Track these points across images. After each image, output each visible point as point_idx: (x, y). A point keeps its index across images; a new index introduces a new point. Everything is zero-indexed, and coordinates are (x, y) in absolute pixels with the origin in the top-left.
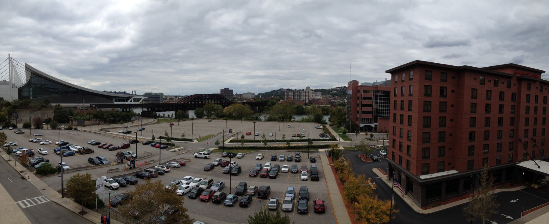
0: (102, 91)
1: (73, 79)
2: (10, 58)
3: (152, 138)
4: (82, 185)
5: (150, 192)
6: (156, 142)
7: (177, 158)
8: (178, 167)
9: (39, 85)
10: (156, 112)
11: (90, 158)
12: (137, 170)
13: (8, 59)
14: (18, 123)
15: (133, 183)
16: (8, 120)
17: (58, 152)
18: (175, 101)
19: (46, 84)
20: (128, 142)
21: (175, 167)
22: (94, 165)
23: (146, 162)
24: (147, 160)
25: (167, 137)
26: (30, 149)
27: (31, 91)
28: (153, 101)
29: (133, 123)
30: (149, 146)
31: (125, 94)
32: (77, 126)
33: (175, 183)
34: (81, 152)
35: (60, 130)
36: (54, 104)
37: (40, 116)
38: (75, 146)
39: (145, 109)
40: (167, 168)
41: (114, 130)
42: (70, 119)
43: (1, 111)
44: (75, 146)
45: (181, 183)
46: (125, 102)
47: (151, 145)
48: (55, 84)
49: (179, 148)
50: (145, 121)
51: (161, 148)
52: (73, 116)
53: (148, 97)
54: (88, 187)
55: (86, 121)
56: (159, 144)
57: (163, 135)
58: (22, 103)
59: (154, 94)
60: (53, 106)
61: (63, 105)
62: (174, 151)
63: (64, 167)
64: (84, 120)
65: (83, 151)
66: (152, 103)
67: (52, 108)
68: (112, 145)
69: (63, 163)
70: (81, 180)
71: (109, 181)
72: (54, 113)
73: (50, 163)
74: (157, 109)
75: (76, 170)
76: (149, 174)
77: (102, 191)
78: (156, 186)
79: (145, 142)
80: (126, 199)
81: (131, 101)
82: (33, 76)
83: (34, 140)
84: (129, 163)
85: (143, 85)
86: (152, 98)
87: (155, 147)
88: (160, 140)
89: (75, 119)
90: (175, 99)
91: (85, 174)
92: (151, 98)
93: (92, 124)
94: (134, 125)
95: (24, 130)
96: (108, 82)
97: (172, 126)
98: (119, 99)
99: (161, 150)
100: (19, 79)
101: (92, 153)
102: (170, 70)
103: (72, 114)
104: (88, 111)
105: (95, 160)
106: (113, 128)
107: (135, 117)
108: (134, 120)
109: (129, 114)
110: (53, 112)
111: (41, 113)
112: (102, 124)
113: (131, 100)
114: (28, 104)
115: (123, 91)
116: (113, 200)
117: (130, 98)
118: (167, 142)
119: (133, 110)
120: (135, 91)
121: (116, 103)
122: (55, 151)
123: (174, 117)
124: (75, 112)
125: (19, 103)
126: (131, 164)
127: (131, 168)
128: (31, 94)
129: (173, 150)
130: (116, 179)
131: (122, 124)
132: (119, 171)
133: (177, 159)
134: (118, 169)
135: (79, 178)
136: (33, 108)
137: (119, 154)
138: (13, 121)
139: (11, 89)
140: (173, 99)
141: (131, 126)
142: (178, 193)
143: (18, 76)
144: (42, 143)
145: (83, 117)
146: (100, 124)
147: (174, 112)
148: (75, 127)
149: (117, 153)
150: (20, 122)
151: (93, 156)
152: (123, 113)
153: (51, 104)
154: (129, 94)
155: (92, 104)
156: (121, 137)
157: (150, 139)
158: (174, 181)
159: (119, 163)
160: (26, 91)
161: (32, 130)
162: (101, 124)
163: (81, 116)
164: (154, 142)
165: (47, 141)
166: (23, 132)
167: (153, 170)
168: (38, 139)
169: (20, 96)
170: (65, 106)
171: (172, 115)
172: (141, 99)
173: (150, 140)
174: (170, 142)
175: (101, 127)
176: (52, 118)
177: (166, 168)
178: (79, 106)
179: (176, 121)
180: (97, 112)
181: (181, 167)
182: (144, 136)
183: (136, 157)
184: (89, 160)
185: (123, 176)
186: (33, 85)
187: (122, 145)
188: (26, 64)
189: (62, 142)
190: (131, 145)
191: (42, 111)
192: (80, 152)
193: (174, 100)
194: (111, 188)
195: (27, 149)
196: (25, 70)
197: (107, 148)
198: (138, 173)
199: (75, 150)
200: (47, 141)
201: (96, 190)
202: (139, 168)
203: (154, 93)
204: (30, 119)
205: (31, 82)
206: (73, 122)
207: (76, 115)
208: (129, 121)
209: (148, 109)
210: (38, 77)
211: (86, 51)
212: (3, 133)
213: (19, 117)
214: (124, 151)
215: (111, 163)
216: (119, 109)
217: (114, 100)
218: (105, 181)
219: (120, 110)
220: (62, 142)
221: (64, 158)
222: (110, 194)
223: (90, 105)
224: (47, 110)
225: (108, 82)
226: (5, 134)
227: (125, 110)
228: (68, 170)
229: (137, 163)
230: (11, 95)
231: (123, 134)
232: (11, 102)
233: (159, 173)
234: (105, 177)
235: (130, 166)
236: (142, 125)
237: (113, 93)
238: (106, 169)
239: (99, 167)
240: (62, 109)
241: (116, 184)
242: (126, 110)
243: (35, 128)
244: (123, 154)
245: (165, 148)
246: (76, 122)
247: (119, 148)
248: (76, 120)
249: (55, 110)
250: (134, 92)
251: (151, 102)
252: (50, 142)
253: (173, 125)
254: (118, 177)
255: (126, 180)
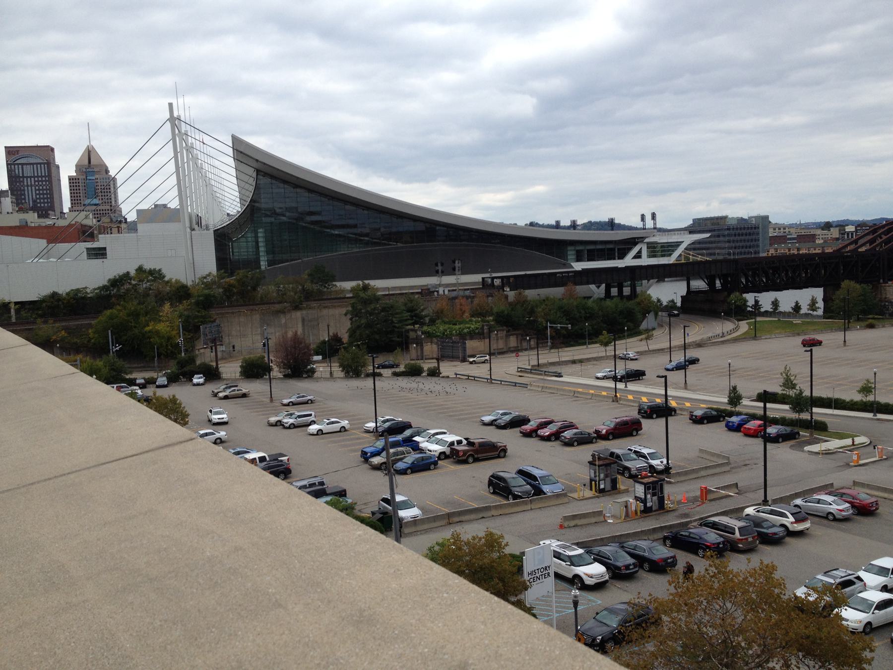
0: (522, 223)
1: (408, 186)
2: (174, 120)
3: (729, 397)
4: (474, 574)
5: (729, 605)
6: (746, 414)
7: (841, 479)
8: (846, 520)
9: (288, 214)
10: (744, 295)
11: (492, 476)
12: (671, 520)
13: (168, 124)
14: (223, 359)
15: (659, 567)
16: (186, 351)
17: (376, 460)
18: (823, 244)
19: (312, 209)
20: (634, 414)
21: (831, 517)
22: (511, 501)
23: (705, 492)
24: (711, 484)
25: (792, 393)
26: (274, 453)
27: (260, 240)
28: (731, 248)
29: (647, 338)
30: (718, 428)
31: (612, 230)
32: (438, 360)
33: (832, 581)
34: (461, 454)
35: (377, 378)
36: (348, 285)
37: (300, 331)
38: (437, 434)
39: (699, 284)
40: (798, 521)
41: (577, 367)
42: (412, 335)
43: (160, 321)
44: (437, 434)
45: (859, 584)
46: (614, 259)
47: (727, 426)
48: (348, 207)
49: (848, 441)
50: (699, 330)
51: (769, 439)
52: (423, 324)
53: (708, 235)
54: (496, 580)
55: (472, 338)
56: (760, 422)
57: (775, 388)
58: (231, 285)
59: (734, 222)
60: (343, 291)
61: (380, 284)
62: (828, 453)
63: (402, 513)
64: (463, 337)
65: (465, 452)
66: (729, 257)
67: (340, 298)
68: (571, 426)
69: (399, 498)
70: (468, 558)
71: (569, 557)
72: (349, 316)
73: (350, 501)
74: (747, 280)
75: (446, 521)
76: (721, 536)
77: (546, 594)
78: (751, 584)
79: (699, 413)
80: (639, 625)
81: (638, 256)
82: (264, 181)
83: (285, 421)
84: (640, 490)
85: (683, 189)
86: (727, 239)
87: (740, 434)
88: (765, 408)
89: (429, 336)
90: (821, 237)
91: (482, 534)
92: (721, 239)
93: (492, 351)
94: (652, 347)
95: (245, 387)
96: (540, 189)
97: (814, 348)
98: (589, 251)
99: (769, 446)
100: (214, 199)
101: (499, 457)
102: (788, 119)
103: (416, 318)
104: (476, 301)
105: (512, 483)
106: (574, 362)
107: (656, 315)
108: (654, 329)
109: (631, 304)
110: (346, 315)
111: (303, 320)
112: (531, 349)
113: (640, 252)
114: (254, 289)
115: (605, 218)
116: (587, 626)
117: (635, 244)
118: (794, 416)
119: (649, 288)
120: (654, 216)
121: (578, 266)
122: (366, 457)
123: (820, 312)
124: (429, 309)
125: (218, 287)
126: (649, 496)
127: (647, 511)
128: (262, 249)
129: (824, 446)
130: (596, 549)
131: (606, 344)
132: (606, 521)
133: (836, 485)
134: (600, 513)
135: (460, 549)
136: (274, 303)
137: (600, 458)
138: (205, 356)
139: (188, 236)
140: (813, 237)
141: (640, 353)
142: (847, 620)
143: (208, 185)
144: (314, 428)
145: (457, 327)
146: (522, 350)
147: (818, 293)
148: (433, 364)
149: (593, 456)
150: (229, 357)
151: (506, 468)
152: (608, 302)
153: (338, 284)
154: (630, 228)
155: (487, 275)
156: (604, 393)
157: (722, 400)
158: (826, 573)
159: (602, 491)
160: (243, 240)
161: (274, 382)
162: (526, 350)
163: (449, 323)
164: (738, 414)
165: (333, 423)
166: (244, 391)
167: (736, 524)
168: (300, 417)
169: (223, 260)
170: (401, 288)
171: (813, 305)
172: (677, 244)
173: (722, 407)
174: (805, 416)
175: (527, 359)
176: (345, 338)
177: (792, 519)
178: (440, 285)
179: (832, 329)
180: (510, 304)
181: (858, 518)
182: (694, 391)
183: (667, 470)
184: (490, 483)
185: (620, 540)
186: (267, 216)
187: (612, 426)
188: (235, 139)
189: (388, 420)
190: (646, 423)
191: (304, 312)
192: (453, 455)
193: (818, 242)
194: (576, 581)
195: (262, 454)
196: (231, 161)
197: (553, 438)
198: (674, 530)
199: (435, 448)
200: (333, 423)
201: (526, 589)
202: (676, 513)
203: (735, 216)
204: (264, 345)
205: (256, 205)
206: (422, 346)
207: (432, 322)
208: (634, 332)
209: (711, 284)
210: (282, 185)
211: (448, 77)
212: (174, 400)
213: (226, 340)
214: (618, 447)
215: (574, 490)
216: (593, 287)
217: (571, 253)
218: (554, 557)
219: (597, 291)
220: (387, 424)
221: (398, 479)
222: (576, 604)
223: (483, 279)
224: (325, 307)
225: (540, 189)
226: (180, 404)
227: (614, 291)
228: (415, 522)
229: (673, 492)
230: (190, 254)
231: (611, 384)
232: (190, 283)
233: (761, 535)
234: (554, 544)
235: (644, 501)
236: (685, 347)
237: (565, 228)
238: (553, 515)
239: (529, 507)
240: (377, 299)
241: (594, 570)
242: (620, 291)
243: (286, 376)
244: (618, 457)
245: (783, 441)
246: (435, 347)
247: (600, 436)
248: (435, 340)
249: (353, 307)
250: (648, 218)
251: (720, 254)
252: (345, 423)
253: (819, 343)
254: (604, 542)
255: (632, 555)
